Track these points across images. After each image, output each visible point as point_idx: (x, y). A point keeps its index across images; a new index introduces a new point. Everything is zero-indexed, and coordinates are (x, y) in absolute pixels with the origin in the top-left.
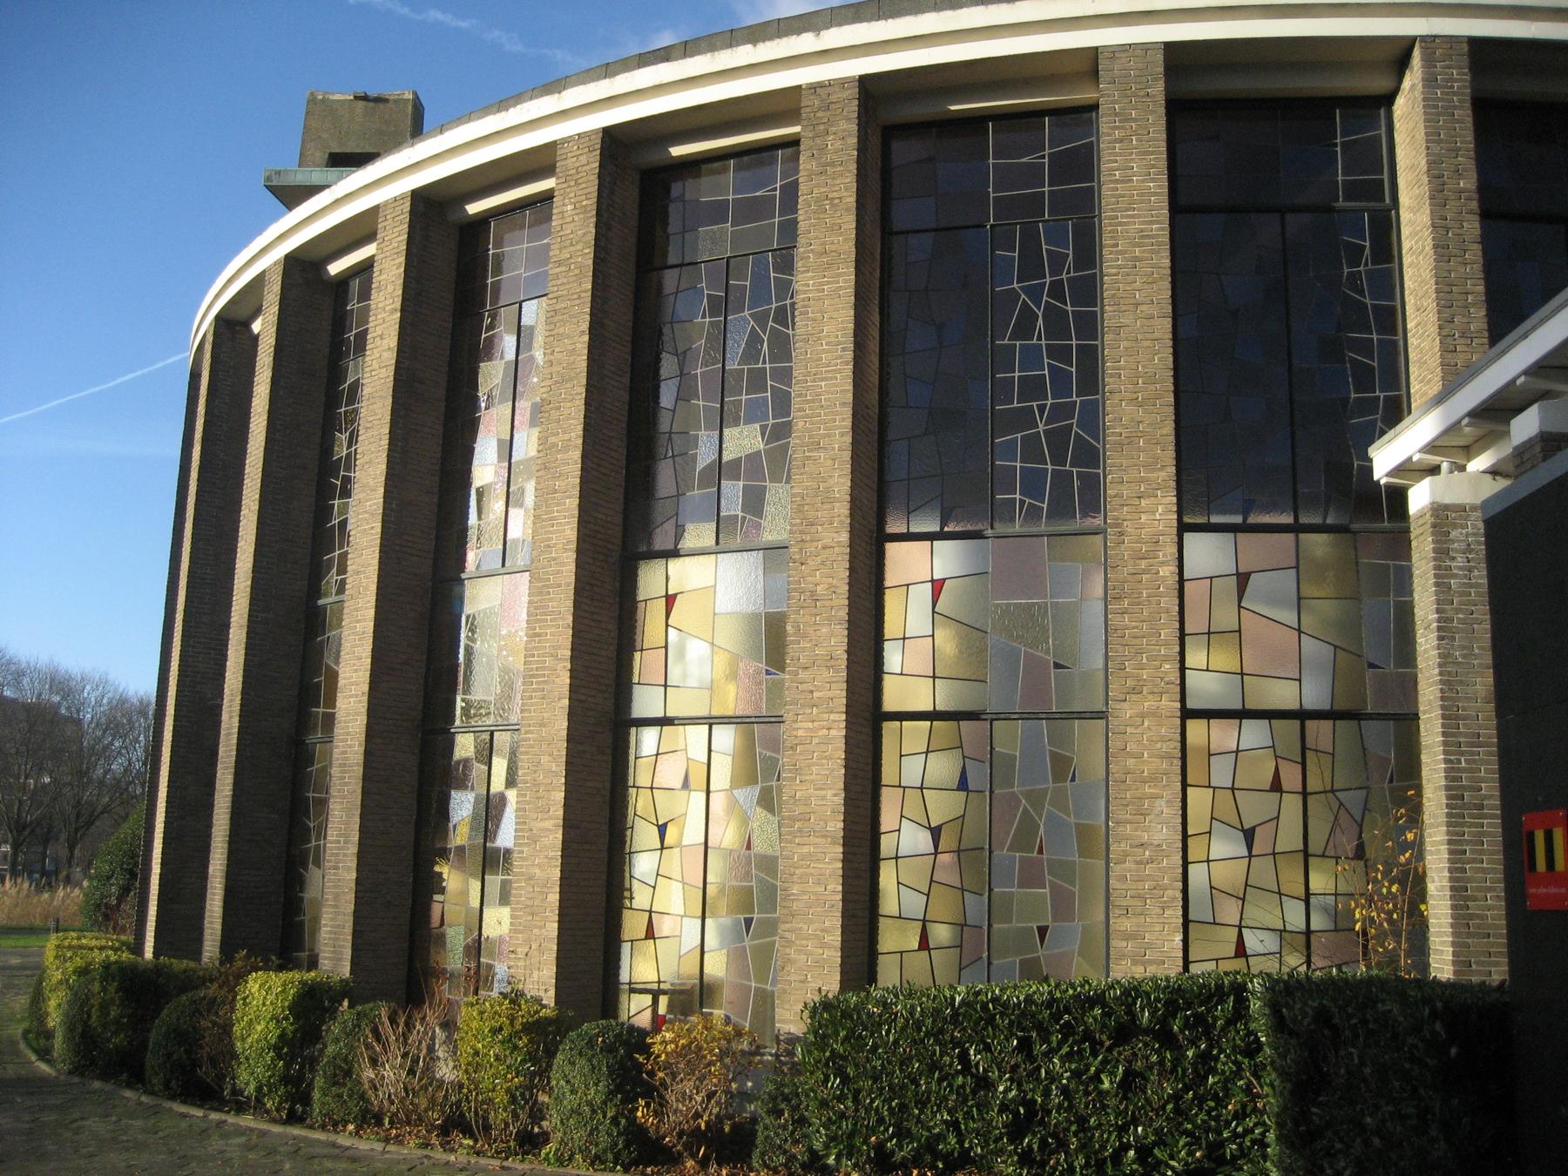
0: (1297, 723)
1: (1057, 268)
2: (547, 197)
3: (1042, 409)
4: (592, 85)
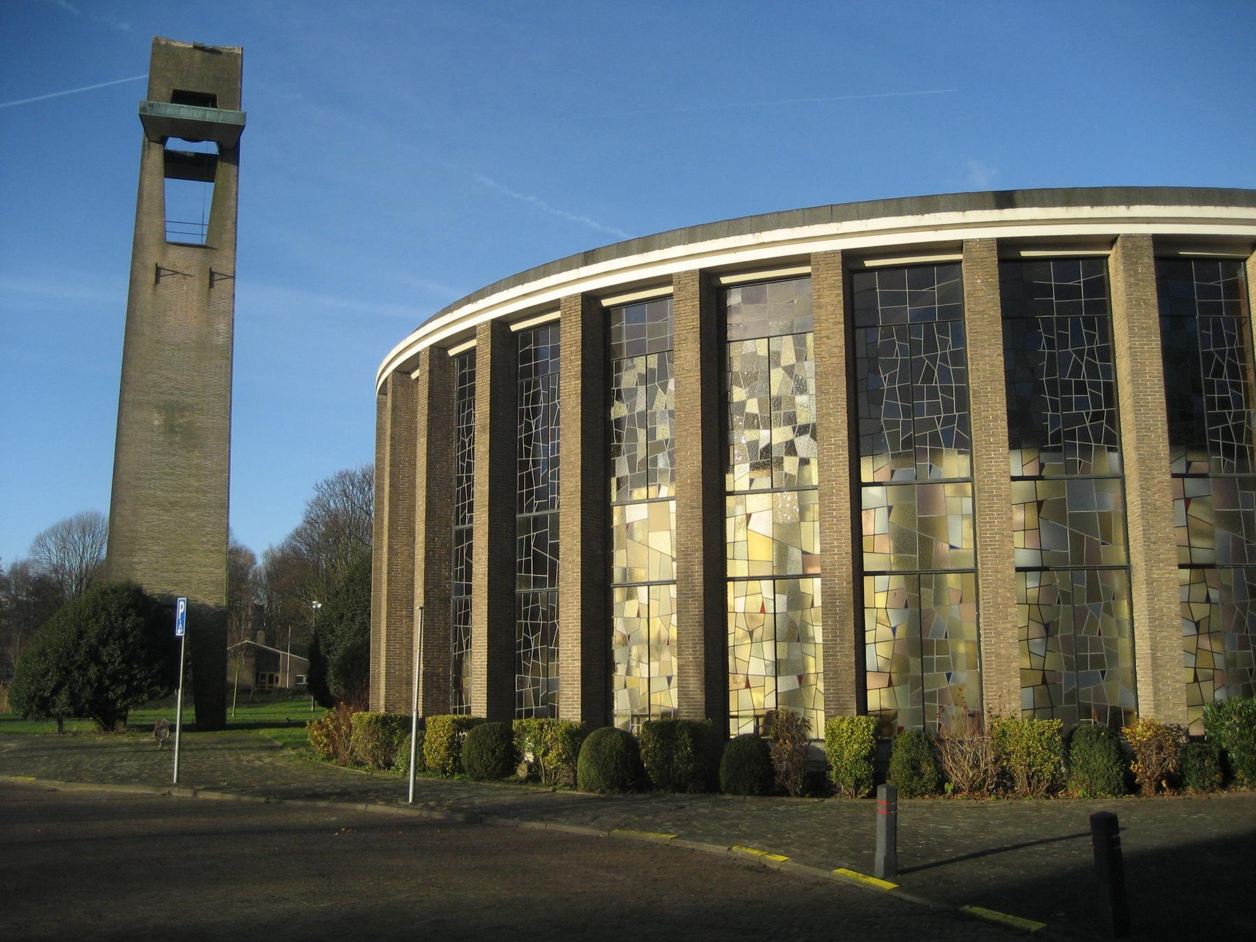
3: (939, 419)
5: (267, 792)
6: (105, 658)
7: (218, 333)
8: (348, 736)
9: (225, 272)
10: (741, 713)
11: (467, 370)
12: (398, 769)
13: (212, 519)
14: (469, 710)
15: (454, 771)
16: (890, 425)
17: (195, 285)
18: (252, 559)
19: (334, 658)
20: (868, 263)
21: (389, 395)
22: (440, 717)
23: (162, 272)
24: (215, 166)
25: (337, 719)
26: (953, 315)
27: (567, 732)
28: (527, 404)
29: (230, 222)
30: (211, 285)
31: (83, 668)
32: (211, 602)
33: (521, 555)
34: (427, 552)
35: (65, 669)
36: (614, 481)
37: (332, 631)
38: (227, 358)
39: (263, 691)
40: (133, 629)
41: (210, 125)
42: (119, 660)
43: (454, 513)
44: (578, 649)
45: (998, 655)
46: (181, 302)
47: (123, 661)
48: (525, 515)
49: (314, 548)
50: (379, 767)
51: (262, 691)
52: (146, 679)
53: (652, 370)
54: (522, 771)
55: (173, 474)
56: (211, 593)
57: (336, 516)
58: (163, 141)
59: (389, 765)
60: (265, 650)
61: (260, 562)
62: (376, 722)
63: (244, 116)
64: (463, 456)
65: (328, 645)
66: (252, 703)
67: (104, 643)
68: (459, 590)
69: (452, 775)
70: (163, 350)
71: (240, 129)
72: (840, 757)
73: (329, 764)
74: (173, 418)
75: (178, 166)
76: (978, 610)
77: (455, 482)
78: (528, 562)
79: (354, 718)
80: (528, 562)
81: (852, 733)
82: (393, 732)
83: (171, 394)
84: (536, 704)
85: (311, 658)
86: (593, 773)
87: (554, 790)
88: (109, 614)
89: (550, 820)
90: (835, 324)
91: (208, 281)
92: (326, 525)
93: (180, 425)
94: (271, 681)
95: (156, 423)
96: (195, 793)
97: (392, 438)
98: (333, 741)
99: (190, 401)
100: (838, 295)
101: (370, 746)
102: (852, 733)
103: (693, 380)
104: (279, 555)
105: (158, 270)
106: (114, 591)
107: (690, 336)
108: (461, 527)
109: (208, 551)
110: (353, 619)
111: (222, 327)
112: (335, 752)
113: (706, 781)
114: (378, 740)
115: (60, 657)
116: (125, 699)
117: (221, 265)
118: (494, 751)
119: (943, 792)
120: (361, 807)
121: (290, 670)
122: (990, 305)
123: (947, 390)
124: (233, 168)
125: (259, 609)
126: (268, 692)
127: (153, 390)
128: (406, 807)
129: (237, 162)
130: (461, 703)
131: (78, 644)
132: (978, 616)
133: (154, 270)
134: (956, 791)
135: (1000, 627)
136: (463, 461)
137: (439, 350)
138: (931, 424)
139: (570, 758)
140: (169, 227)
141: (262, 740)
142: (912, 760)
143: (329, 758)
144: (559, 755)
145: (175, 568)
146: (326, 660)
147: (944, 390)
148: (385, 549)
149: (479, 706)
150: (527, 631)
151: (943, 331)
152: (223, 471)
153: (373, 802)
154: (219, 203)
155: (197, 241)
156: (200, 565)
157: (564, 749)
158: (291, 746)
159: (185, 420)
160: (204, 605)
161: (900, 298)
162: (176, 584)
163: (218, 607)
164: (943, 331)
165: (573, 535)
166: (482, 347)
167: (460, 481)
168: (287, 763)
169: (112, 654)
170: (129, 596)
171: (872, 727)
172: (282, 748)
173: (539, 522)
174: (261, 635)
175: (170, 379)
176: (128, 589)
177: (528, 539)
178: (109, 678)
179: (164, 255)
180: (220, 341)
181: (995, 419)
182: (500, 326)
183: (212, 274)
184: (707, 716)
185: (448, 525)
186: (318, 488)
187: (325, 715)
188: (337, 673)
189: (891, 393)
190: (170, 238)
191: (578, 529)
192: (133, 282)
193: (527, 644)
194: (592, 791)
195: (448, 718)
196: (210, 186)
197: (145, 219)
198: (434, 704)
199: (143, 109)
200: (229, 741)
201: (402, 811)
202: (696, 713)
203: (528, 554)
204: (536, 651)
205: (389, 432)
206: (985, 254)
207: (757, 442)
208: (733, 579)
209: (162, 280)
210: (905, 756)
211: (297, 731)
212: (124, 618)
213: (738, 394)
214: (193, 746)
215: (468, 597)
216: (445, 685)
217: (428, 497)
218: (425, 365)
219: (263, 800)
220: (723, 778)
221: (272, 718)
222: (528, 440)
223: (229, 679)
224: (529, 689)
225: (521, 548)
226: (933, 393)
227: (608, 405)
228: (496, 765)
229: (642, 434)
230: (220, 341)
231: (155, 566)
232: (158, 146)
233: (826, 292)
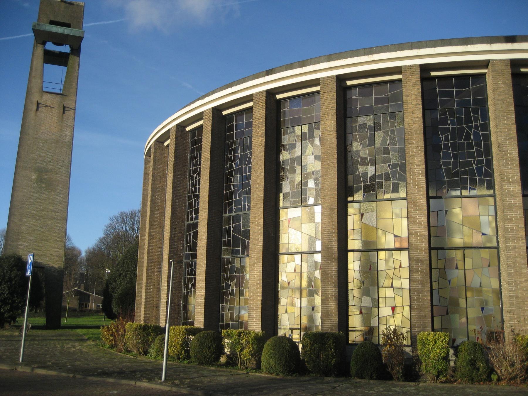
0: (431, 200)
1: (476, 121)
2: (251, 108)
3: (474, 161)
4: (362, 57)
5: (75, 370)
7: (66, 136)
8: (123, 336)
10: (356, 329)
11: (196, 138)
12: (151, 356)
13: (59, 225)
14: (192, 323)
15: (184, 358)
16: (445, 164)
17: (55, 113)
18: (80, 253)
19: (116, 295)
20: (433, 74)
21: (152, 157)
22: (177, 327)
23: (40, 105)
24: (68, 58)
25: (118, 326)
26: (481, 104)
27: (255, 338)
28: (231, 154)
30: (64, 113)
32: (56, 266)
33: (226, 238)
34: (171, 235)
36: (281, 195)
37: (115, 281)
38: (70, 148)
39: (82, 310)
40: (15, 277)
41: (67, 36)
42: (7, 292)
43: (186, 215)
44: (260, 290)
45: (517, 297)
46: (48, 121)
47: (9, 293)
48: (228, 215)
49: (108, 247)
50: (140, 354)
51: (81, 311)
53: (305, 133)
54: (223, 360)
55: (40, 202)
56: (56, 261)
57: (118, 234)
58: (44, 43)
59: (146, 353)
60: (84, 293)
61: (84, 254)
62: (140, 328)
63: (83, 33)
64: (192, 184)
65: (113, 289)
66: (77, 316)
68: (188, 257)
69: (183, 360)
70: (39, 143)
71: (81, 38)
72: (428, 357)
73: (112, 351)
74: (44, 177)
75: (51, 58)
76: (499, 270)
77: (187, 198)
78: (229, 241)
79: (127, 326)
80: (229, 241)
81: (435, 343)
82: (149, 334)
83: (42, 164)
84: (232, 321)
85: (104, 296)
86: (272, 363)
87: (248, 373)
88: (3, 270)
90: (416, 105)
91: (62, 111)
92: (113, 236)
93: (45, 179)
94: (86, 307)
95: (33, 177)
96: (33, 369)
97: (153, 176)
98: (115, 338)
99: (50, 167)
100: (418, 89)
101: (135, 342)
102: (435, 343)
103: (332, 136)
104: (92, 250)
105: (38, 104)
106: (7, 258)
107: (330, 112)
108: (190, 222)
109: (56, 240)
110: (126, 276)
111: (68, 133)
112: (115, 344)
113: (342, 370)
114: (140, 338)
116: (9, 312)
117: (69, 103)
118: (209, 348)
119: (490, 380)
120: (133, 383)
121: (95, 302)
122: (507, 96)
123: (479, 145)
124: (77, 58)
125: (82, 275)
126: (85, 311)
128: (161, 384)
129: (79, 56)
130: (187, 319)
132: (500, 275)
134: (499, 380)
135: (518, 280)
136: (192, 186)
137: (181, 127)
138: (469, 164)
139: (257, 354)
140: (45, 85)
141: (78, 335)
142: (472, 360)
143: (112, 347)
144: (250, 351)
145: (39, 248)
146: (112, 296)
147: (477, 145)
148: (147, 235)
149: (199, 322)
150: (227, 280)
151: (476, 112)
152: (65, 202)
153: (140, 379)
154: (68, 75)
155: (58, 92)
156: (52, 247)
157: (253, 348)
158: (92, 341)
159: (47, 176)
160: (53, 267)
161: (451, 94)
163: (60, 268)
164: (476, 112)
165: (258, 224)
166: (207, 124)
167: (190, 198)
168: (89, 348)
171: (447, 339)
172: (87, 340)
173: (236, 219)
174: (82, 286)
175: (41, 156)
177: (230, 228)
179: (42, 97)
180: (67, 139)
181: (512, 160)
182: (217, 111)
183: (64, 107)
184: (339, 330)
185: (183, 221)
186: (110, 219)
187: (111, 323)
188: (119, 301)
189: (446, 146)
190: (45, 89)
191: (261, 221)
192: (26, 109)
193: (228, 286)
194: (271, 374)
195: (182, 328)
196: (65, 68)
197: (33, 80)
198: (173, 321)
199: (34, 26)
200: (61, 335)
201: (158, 387)
202: (332, 328)
203: (229, 236)
204: (233, 291)
205: (151, 173)
206: (504, 68)
207: (367, 173)
208: (353, 251)
209: (40, 109)
210: (468, 357)
211: (96, 331)
212: (11, 271)
213: (356, 146)
214: (40, 338)
215: (193, 261)
216: (180, 311)
217: (172, 205)
218: (173, 136)
219: (71, 375)
220: (353, 369)
221: (84, 323)
222: (231, 174)
223: (63, 304)
224: (227, 313)
225: (225, 234)
226: (470, 146)
227: (278, 153)
228: (211, 356)
229: (298, 169)
230: (67, 139)
231: (29, 247)
232: (41, 46)
233: (411, 88)
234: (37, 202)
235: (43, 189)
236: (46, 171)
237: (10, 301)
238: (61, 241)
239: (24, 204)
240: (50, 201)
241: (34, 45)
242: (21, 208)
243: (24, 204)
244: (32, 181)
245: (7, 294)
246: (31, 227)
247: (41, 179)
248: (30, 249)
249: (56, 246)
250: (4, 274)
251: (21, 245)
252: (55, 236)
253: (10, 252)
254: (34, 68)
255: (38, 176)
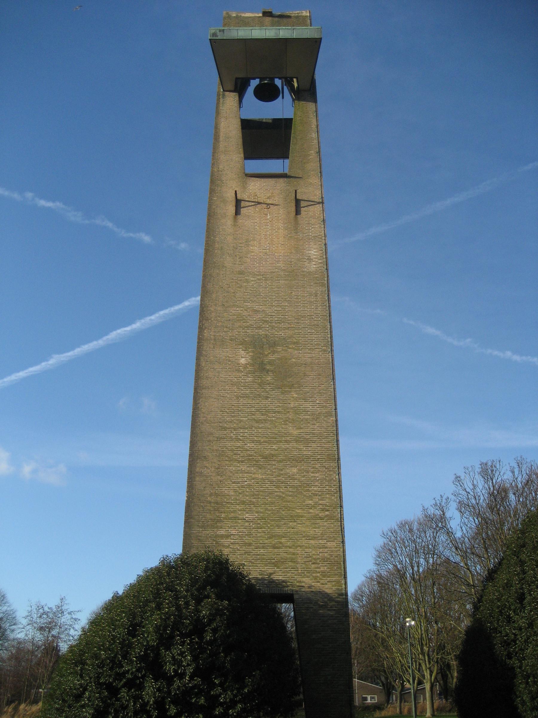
6: (170, 668)
7: (310, 260)
9: (311, 198)
17: (281, 213)
23: (243, 204)
29: (313, 153)
30: (298, 212)
31: (136, 685)
35: (109, 687)
38: (323, 285)
42: (190, 670)
52: (233, 704)
56: (324, 574)
65: (507, 644)
67: (166, 642)
70: (247, 281)
71: (312, 46)
83: (260, 328)
89: (354, 688)
91: (293, 209)
93: (271, 363)
95: (243, 361)
99: (282, 333)
105: (238, 203)
109: (316, 517)
115: (101, 665)
124: (311, 106)
127: (237, 324)
129: (315, 101)
131: (130, 645)
133: (234, 203)
145: (275, 541)
152: (329, 414)
156: (309, 538)
159: (276, 356)
162: (275, 565)
169: (180, 658)
170: (207, 568)
175: (256, 311)
176: (207, 560)
178: (174, 702)
180: (313, 267)
186: (384, 535)
192: (211, 215)
209: (243, 211)
212: (199, 601)
231: (247, 540)
234: (257, 421)
235: (268, 388)
236: (274, 345)
237: (202, 701)
238: (330, 517)
239: (225, 429)
240: (291, 416)
241: (218, 95)
242: (219, 439)
243: (225, 429)
244: (239, 371)
245: (191, 678)
246: (249, 486)
247: (262, 363)
248: (250, 544)
249: (319, 531)
250: (178, 608)
251: (228, 536)
252: (313, 507)
253: (198, 549)
254: (222, 134)
255: (253, 358)
